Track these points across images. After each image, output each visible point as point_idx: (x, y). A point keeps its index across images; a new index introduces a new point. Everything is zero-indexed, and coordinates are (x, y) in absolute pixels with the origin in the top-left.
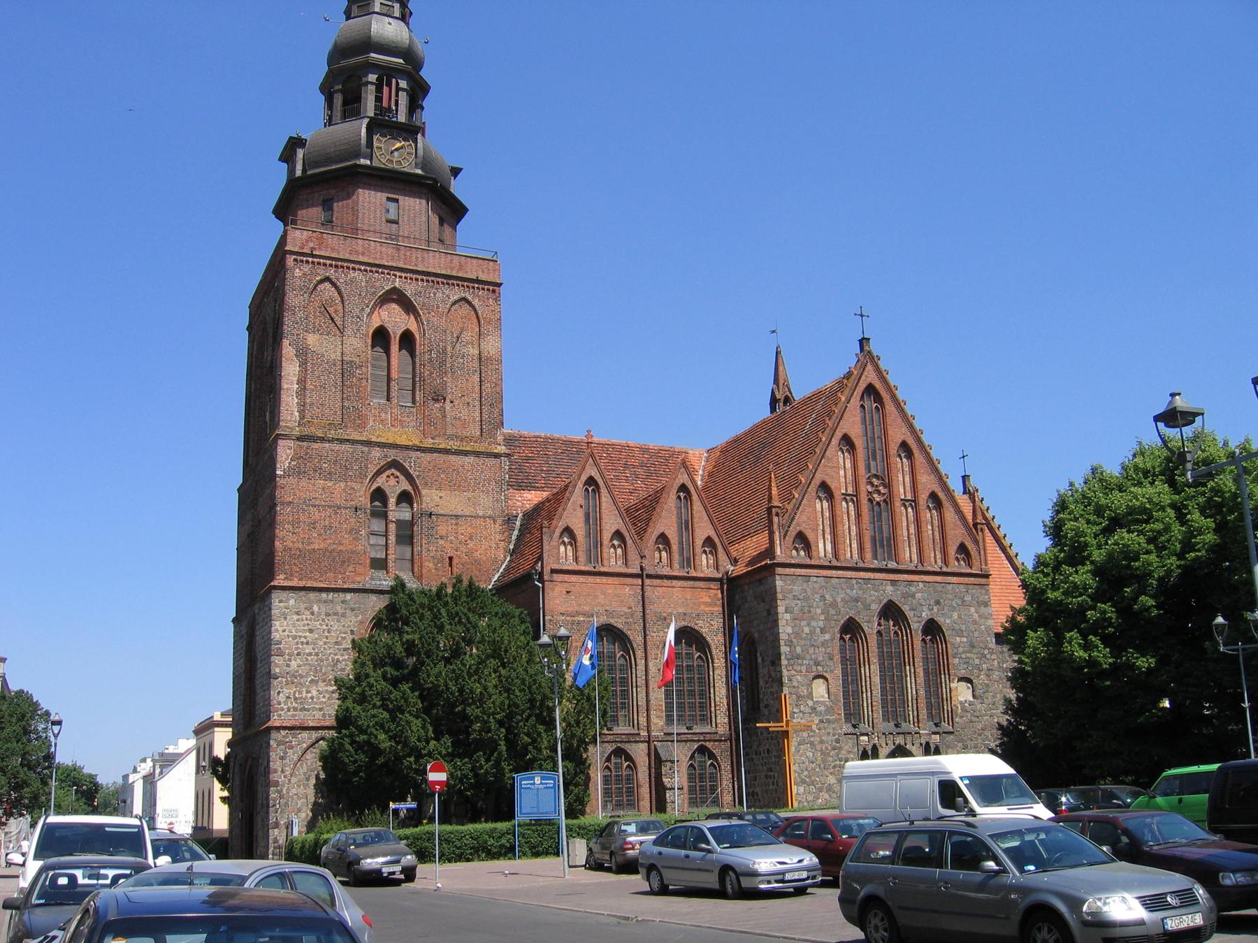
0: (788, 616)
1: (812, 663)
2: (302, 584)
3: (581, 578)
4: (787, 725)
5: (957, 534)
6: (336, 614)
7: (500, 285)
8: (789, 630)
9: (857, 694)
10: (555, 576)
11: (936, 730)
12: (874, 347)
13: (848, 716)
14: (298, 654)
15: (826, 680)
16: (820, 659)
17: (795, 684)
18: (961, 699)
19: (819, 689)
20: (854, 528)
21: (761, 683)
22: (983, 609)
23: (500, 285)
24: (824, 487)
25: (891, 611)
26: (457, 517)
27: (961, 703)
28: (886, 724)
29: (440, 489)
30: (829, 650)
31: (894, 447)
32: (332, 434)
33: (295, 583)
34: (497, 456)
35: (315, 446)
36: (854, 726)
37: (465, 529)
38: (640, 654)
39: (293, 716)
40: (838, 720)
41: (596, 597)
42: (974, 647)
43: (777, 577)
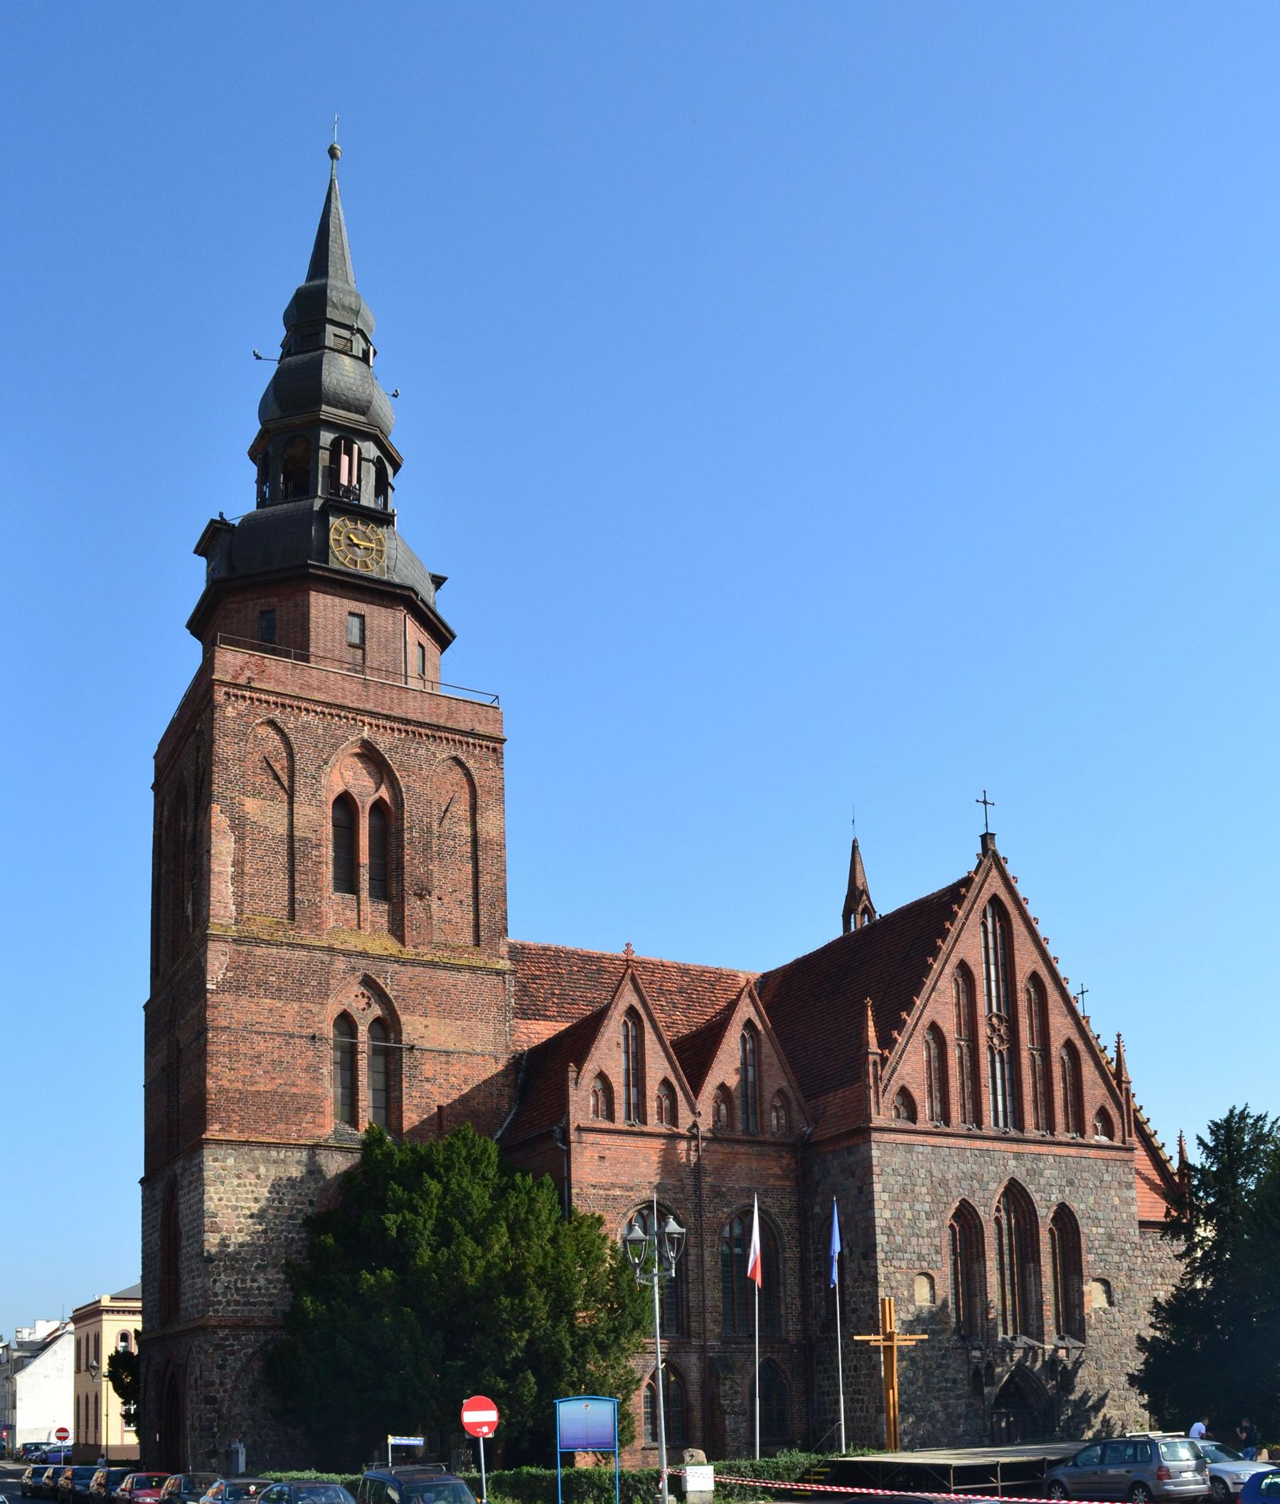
0: (885, 1196)
8: (887, 1214)
12: (1001, 847)
26: (448, 1053)
41: (637, 1165)
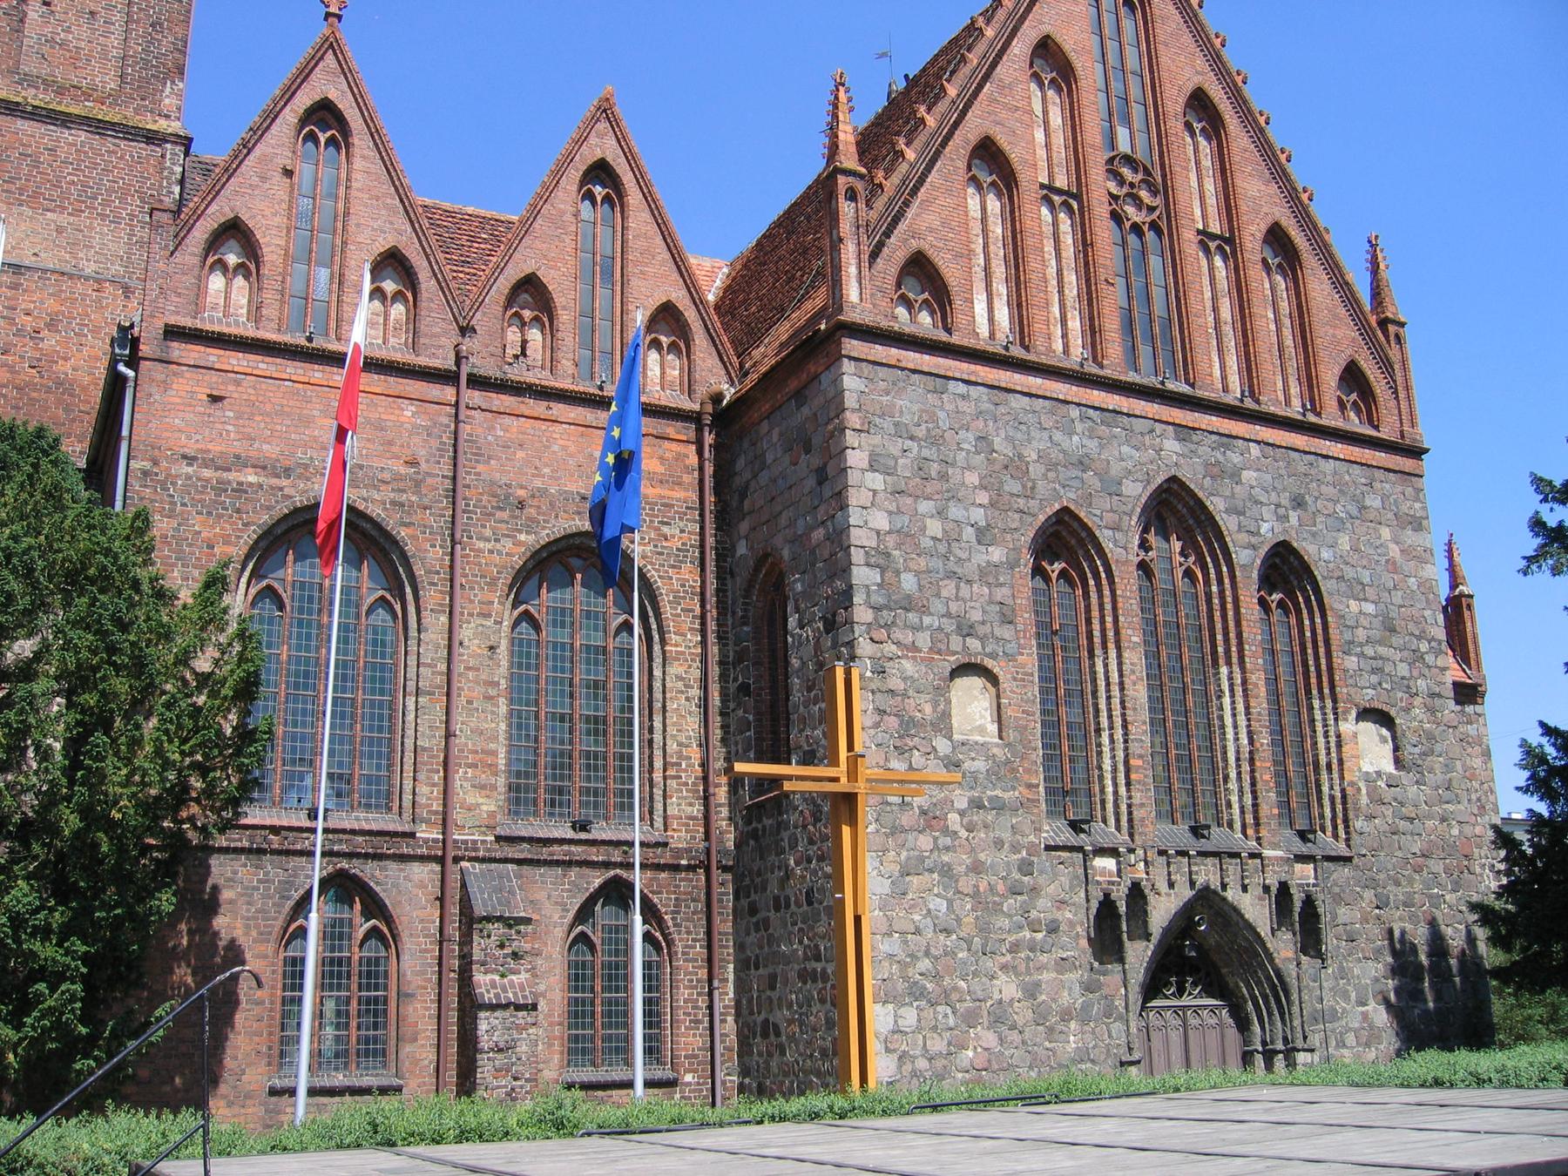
0: (876, 481)
1: (949, 625)
3: (263, 364)
4: (853, 774)
5: (1338, 341)
8: (881, 521)
9: (1086, 733)
10: (178, 350)
11: (1305, 849)
13: (1058, 795)
15: (993, 679)
16: (976, 616)
17: (895, 683)
18: (1367, 767)
19: (971, 707)
20: (1071, 278)
21: (797, 696)
22: (1410, 537)
24: (988, 153)
25: (1175, 510)
27: (1367, 778)
28: (1166, 827)
30: (1002, 593)
31: (1174, 103)
34: (153, 138)
36: (1076, 826)
38: (433, 596)
40: (1023, 805)
42: (1393, 630)
43: (847, 366)
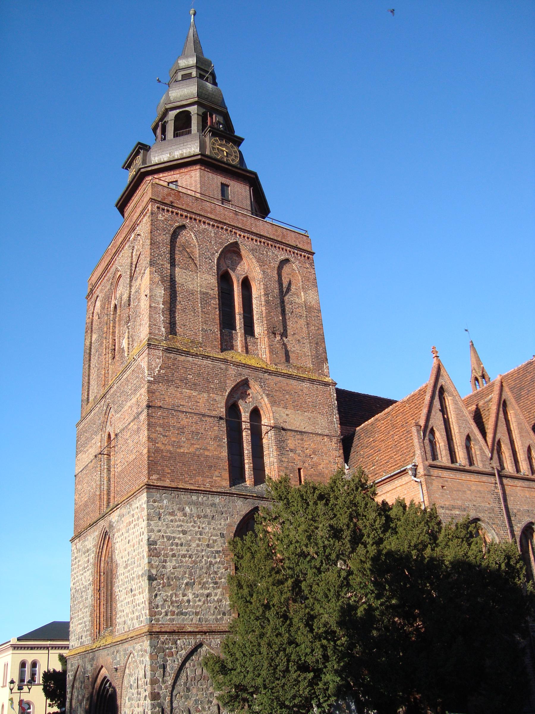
2: (174, 485)
6: (205, 516)
7: (314, 253)
14: (174, 555)
23: (313, 254)
26: (301, 432)
29: (286, 407)
32: (193, 350)
33: (167, 483)
35: (182, 358)
37: (310, 444)
39: (172, 620)
